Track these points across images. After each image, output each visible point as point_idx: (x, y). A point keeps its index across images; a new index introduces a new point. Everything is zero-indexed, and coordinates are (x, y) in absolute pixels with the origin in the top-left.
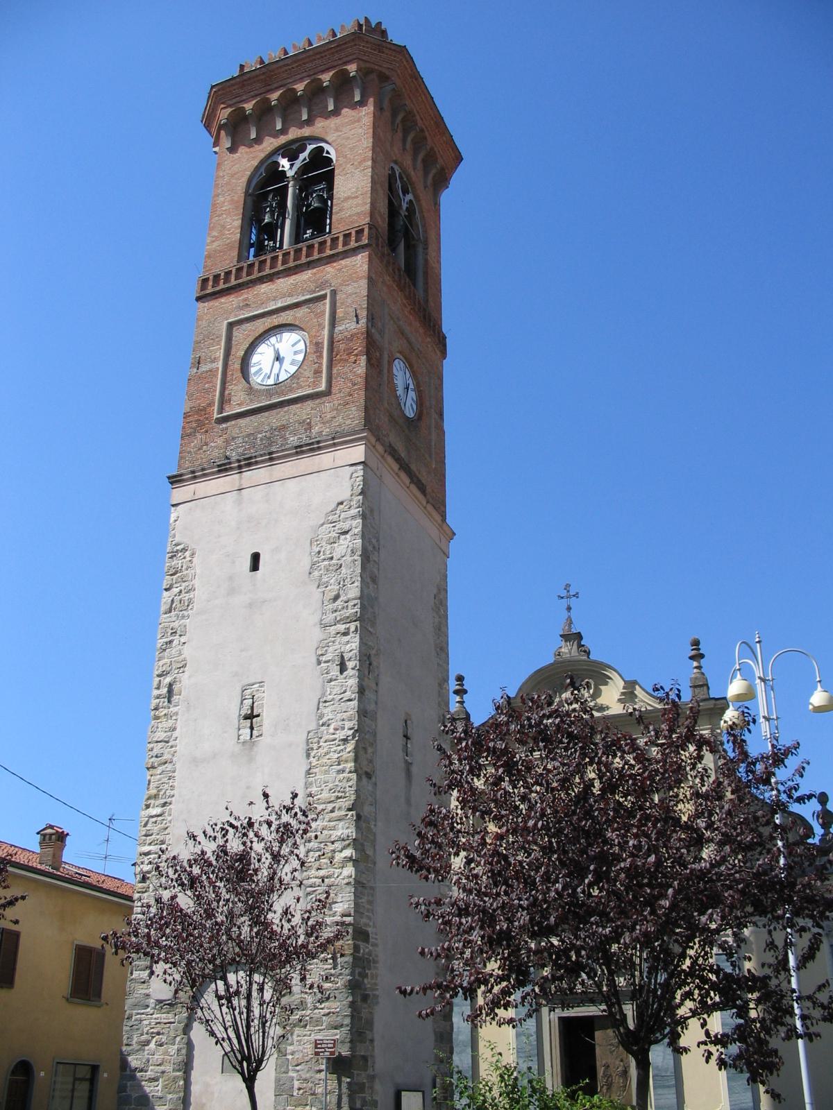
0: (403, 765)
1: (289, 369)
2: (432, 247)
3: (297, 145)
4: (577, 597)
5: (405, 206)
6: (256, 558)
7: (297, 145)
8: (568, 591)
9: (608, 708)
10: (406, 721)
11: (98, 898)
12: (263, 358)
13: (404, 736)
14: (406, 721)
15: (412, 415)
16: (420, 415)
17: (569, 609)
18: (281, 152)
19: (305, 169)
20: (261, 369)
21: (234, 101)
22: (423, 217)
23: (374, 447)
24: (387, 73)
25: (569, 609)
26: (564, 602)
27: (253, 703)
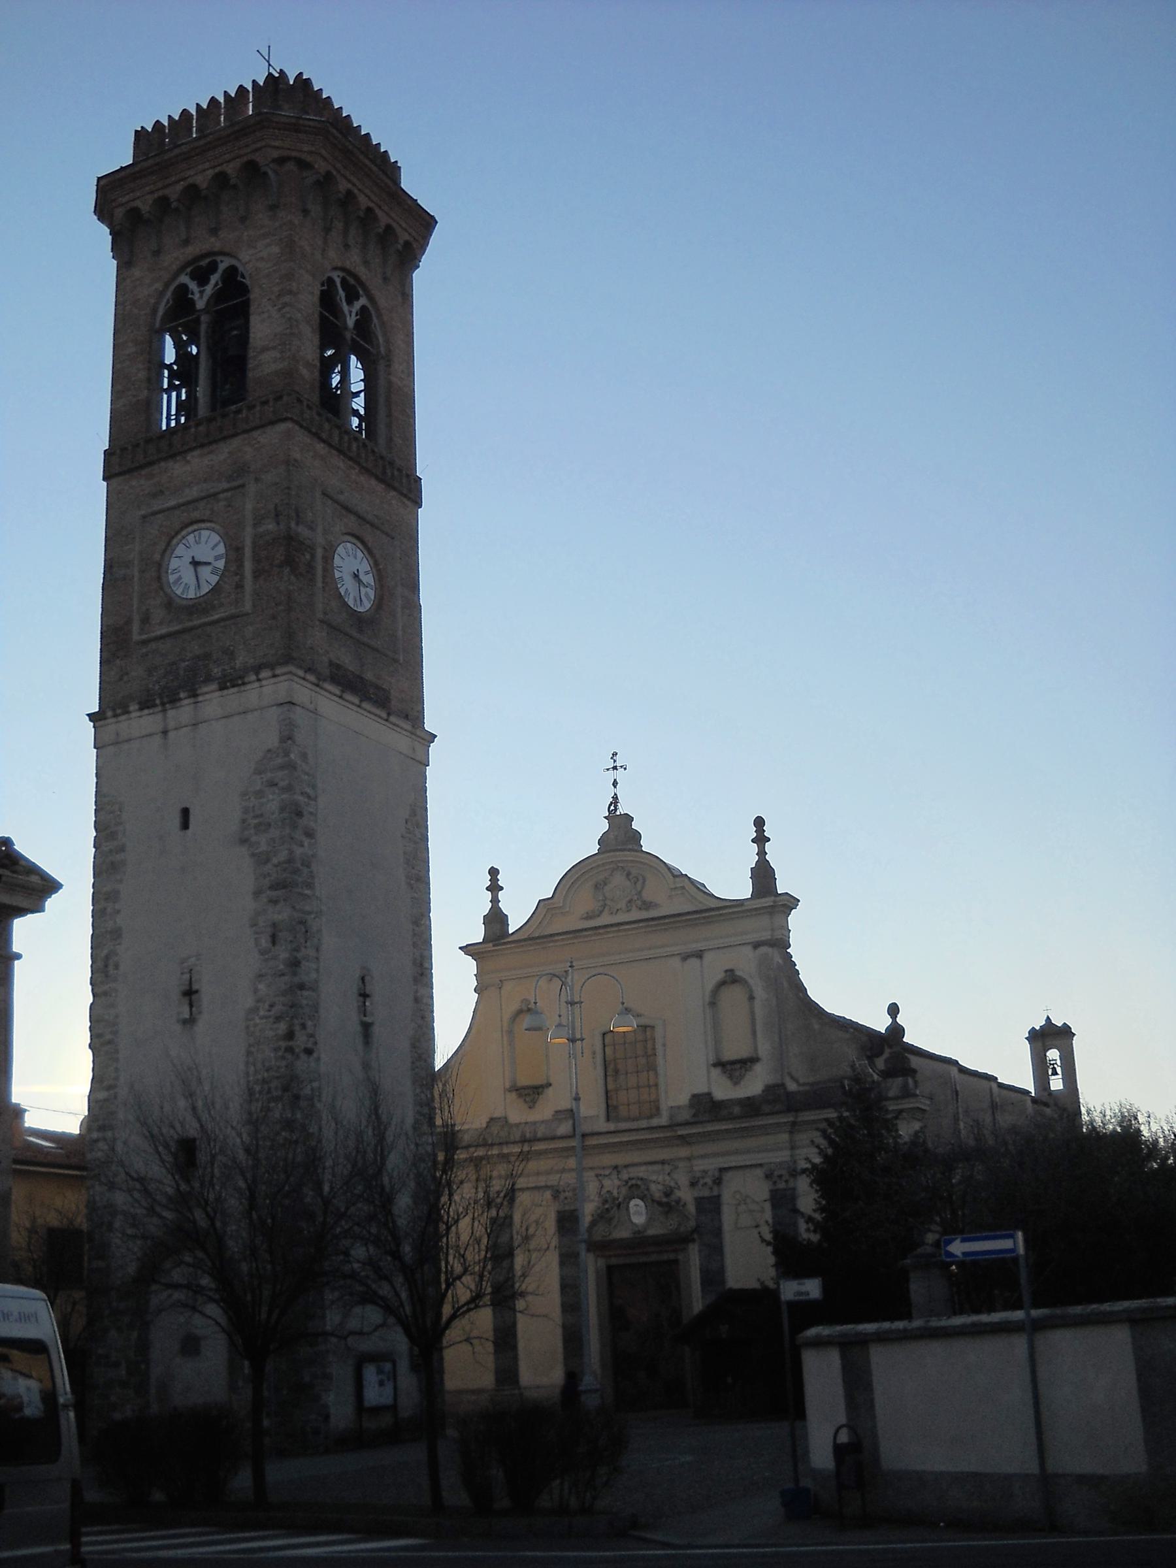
0: (359, 1028)
1: (209, 578)
2: (397, 366)
3: (207, 260)
4: (625, 769)
5: (351, 322)
6: (185, 812)
7: (207, 260)
8: (615, 761)
9: (656, 905)
10: (363, 979)
11: (60, 1174)
12: (179, 567)
13: (361, 995)
14: (363, 979)
15: (365, 607)
16: (379, 603)
17: (615, 784)
18: (189, 270)
19: (218, 296)
20: (180, 578)
21: (127, 198)
22: (383, 324)
23: (304, 679)
24: (309, 159)
25: (615, 784)
26: (612, 775)
27: (191, 979)
